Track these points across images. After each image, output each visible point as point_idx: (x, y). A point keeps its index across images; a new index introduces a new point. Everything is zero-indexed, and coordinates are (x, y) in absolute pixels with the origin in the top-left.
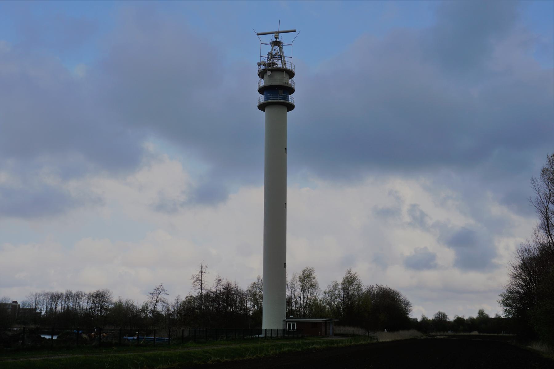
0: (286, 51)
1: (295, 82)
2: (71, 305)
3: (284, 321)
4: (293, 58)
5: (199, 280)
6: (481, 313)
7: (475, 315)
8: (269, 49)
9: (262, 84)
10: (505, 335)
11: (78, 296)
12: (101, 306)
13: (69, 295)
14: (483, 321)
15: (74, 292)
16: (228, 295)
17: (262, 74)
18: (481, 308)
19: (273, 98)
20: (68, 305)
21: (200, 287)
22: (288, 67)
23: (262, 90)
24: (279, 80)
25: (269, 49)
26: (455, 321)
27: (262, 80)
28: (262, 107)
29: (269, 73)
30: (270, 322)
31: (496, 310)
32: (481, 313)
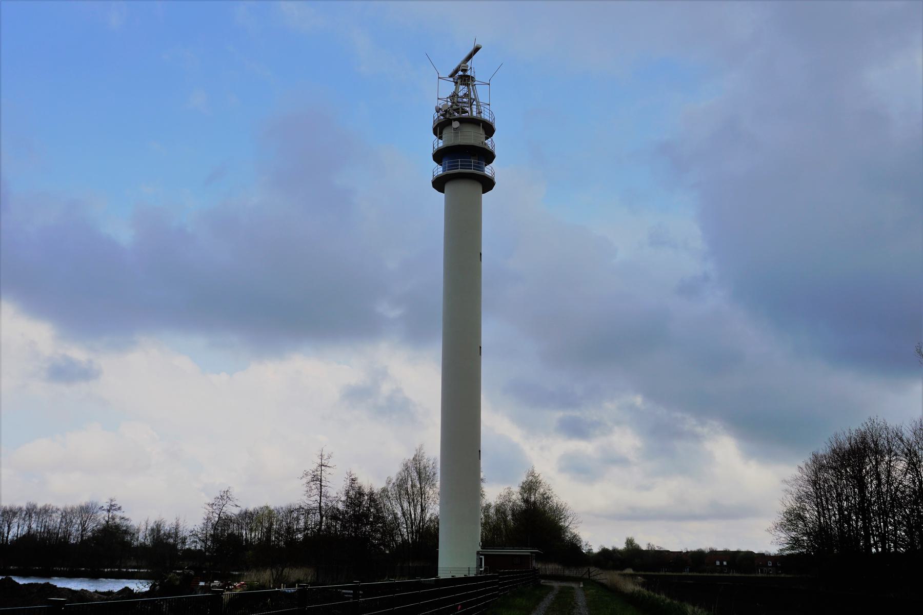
0: (481, 93)
1: (496, 143)
2: (34, 526)
3: (478, 553)
4: (490, 102)
5: (317, 479)
6: (630, 542)
7: (621, 546)
8: (449, 88)
9: (441, 144)
10: (668, 574)
11: (46, 511)
12: (878, 493)
13: (31, 512)
14: (615, 551)
15: (40, 505)
16: (361, 511)
17: (439, 129)
18: (630, 536)
19: (463, 166)
20: (30, 527)
21: (318, 493)
22: (486, 116)
23: (439, 156)
24: (471, 136)
25: (449, 88)
26: (599, 553)
27: (440, 141)
28: (439, 184)
29: (456, 124)
30: (456, 559)
31: (765, 538)
32: (630, 542)
